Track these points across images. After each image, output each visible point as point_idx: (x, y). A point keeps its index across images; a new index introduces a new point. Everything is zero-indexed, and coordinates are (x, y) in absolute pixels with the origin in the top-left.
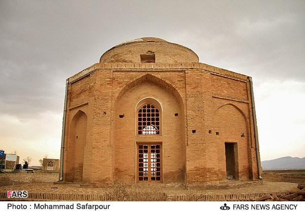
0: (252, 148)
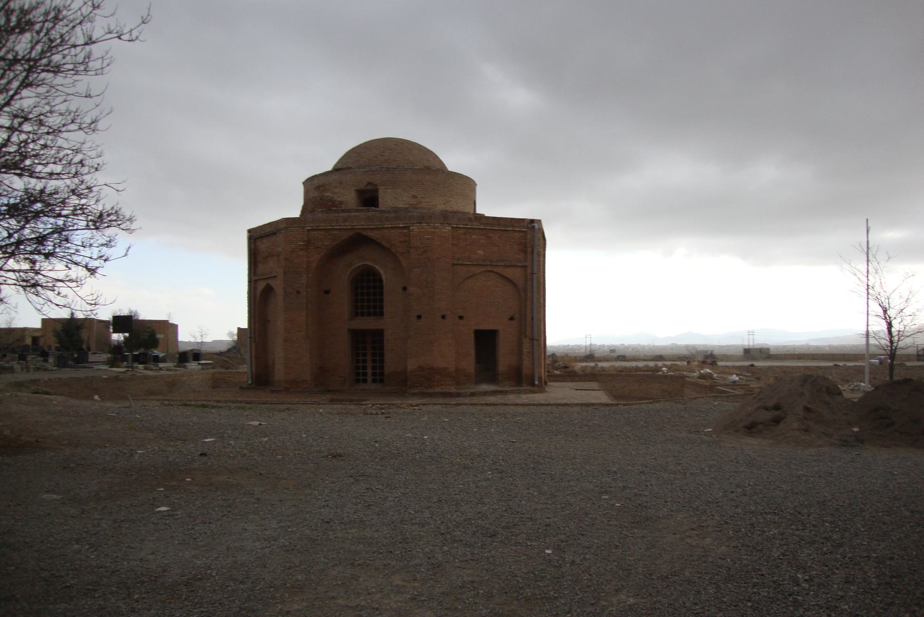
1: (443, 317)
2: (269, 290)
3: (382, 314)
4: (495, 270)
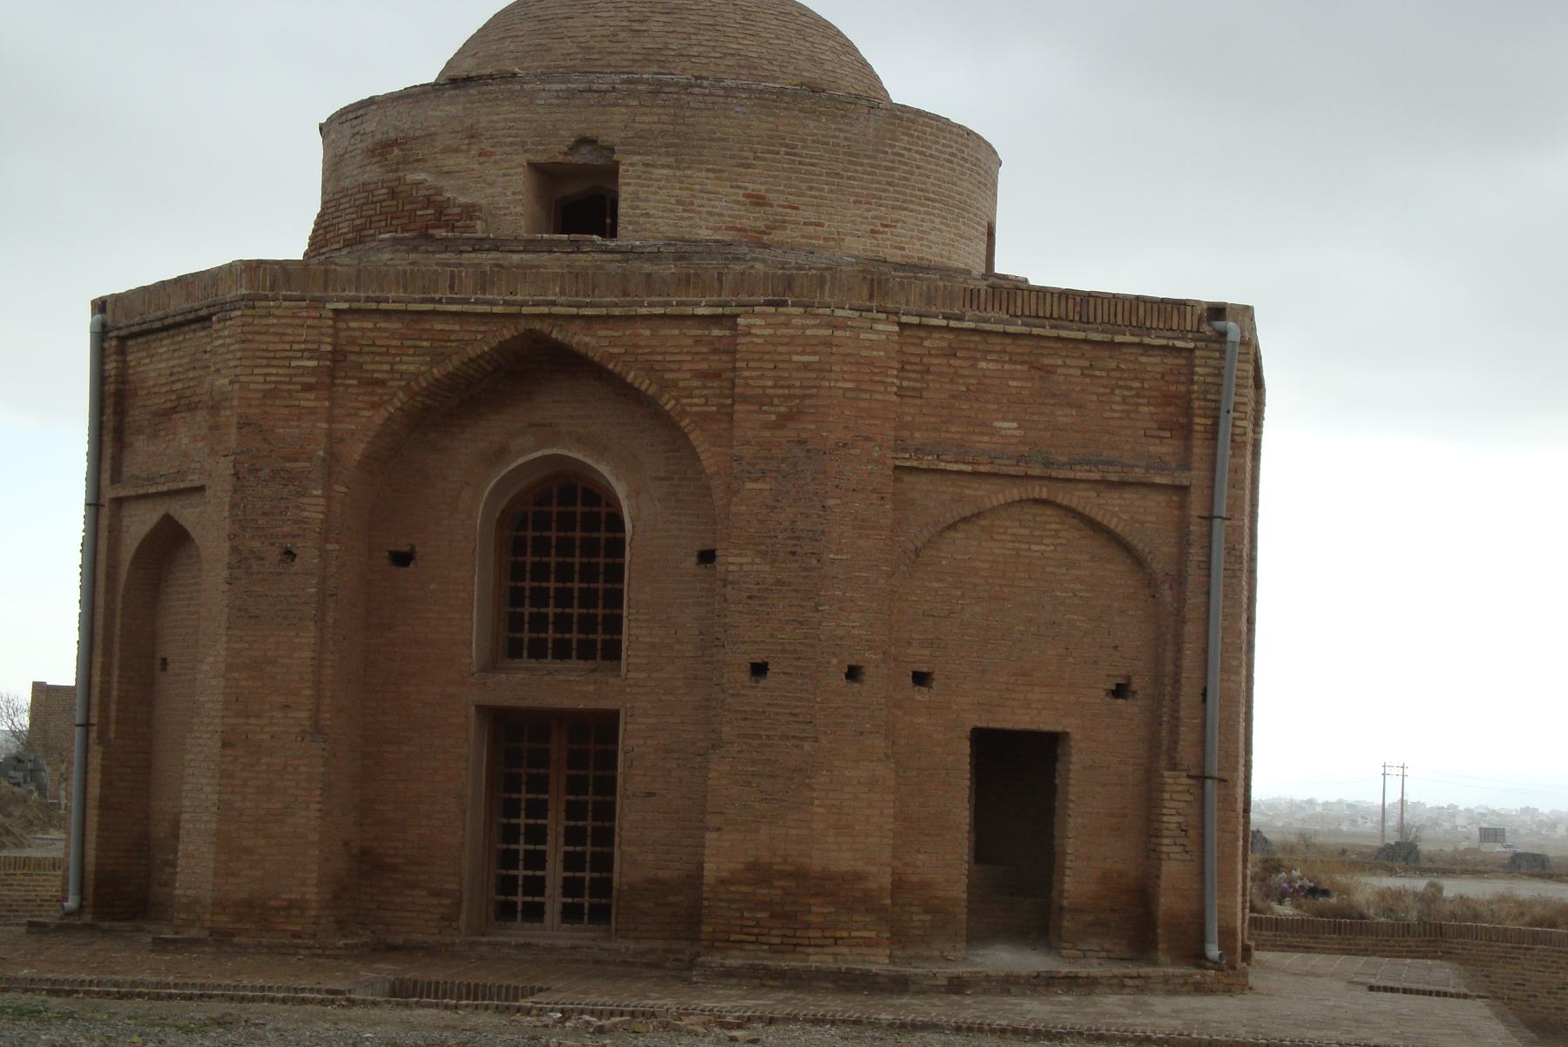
0: (1173, 767)
1: (853, 673)
2: (170, 542)
3: (613, 652)
4: (1062, 498)
